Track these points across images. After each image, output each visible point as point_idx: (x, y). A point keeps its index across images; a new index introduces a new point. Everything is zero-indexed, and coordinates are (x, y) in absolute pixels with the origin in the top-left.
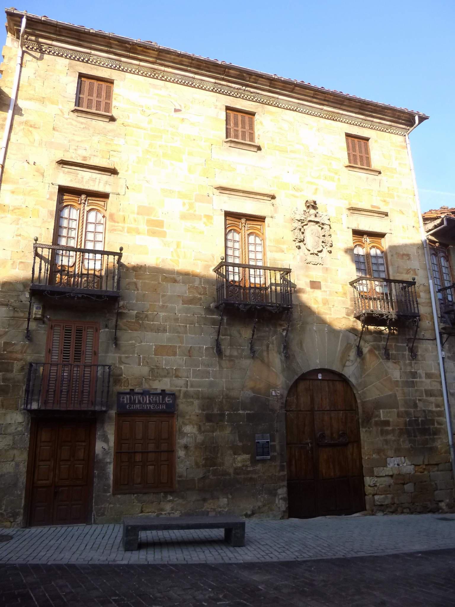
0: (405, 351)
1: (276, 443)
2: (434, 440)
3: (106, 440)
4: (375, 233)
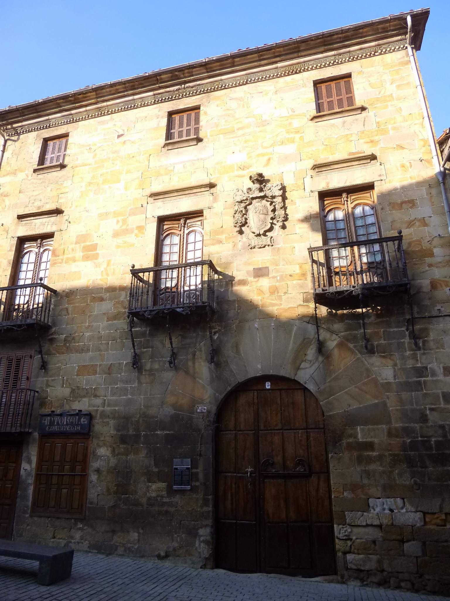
0: (404, 337)
1: (200, 470)
3: (29, 462)
4: (356, 187)
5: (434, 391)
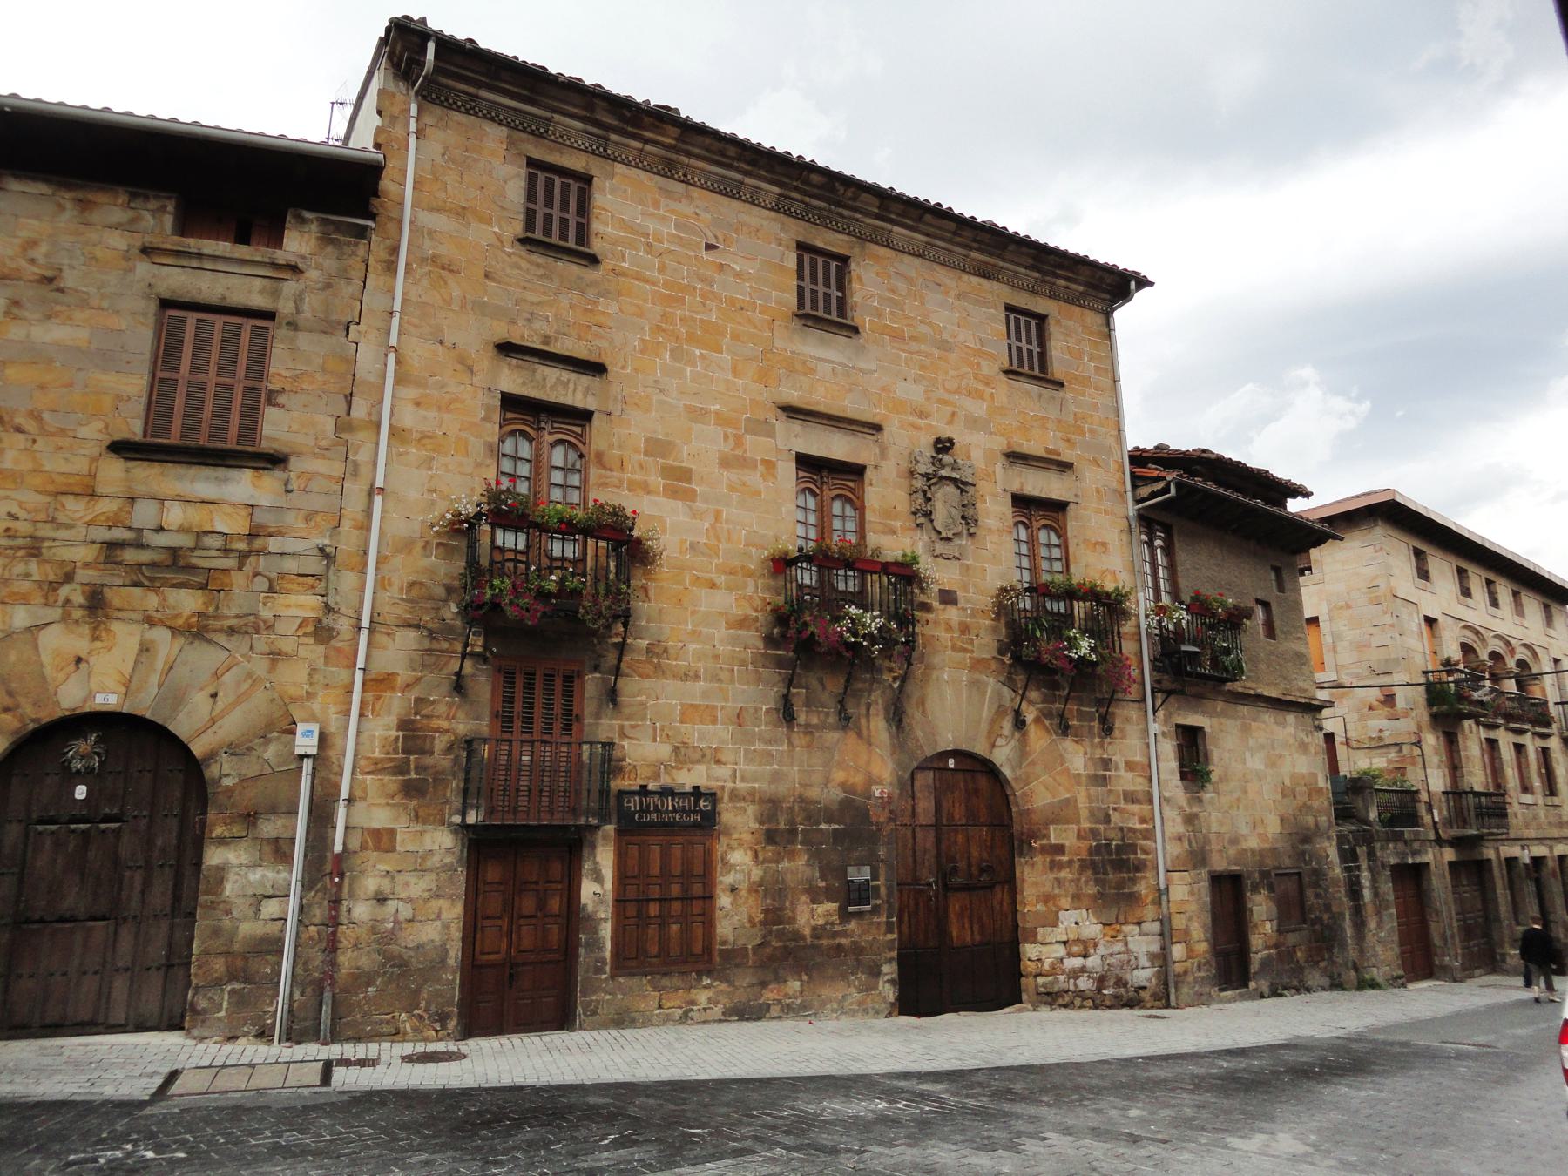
2: (1133, 881)
3: (598, 878)
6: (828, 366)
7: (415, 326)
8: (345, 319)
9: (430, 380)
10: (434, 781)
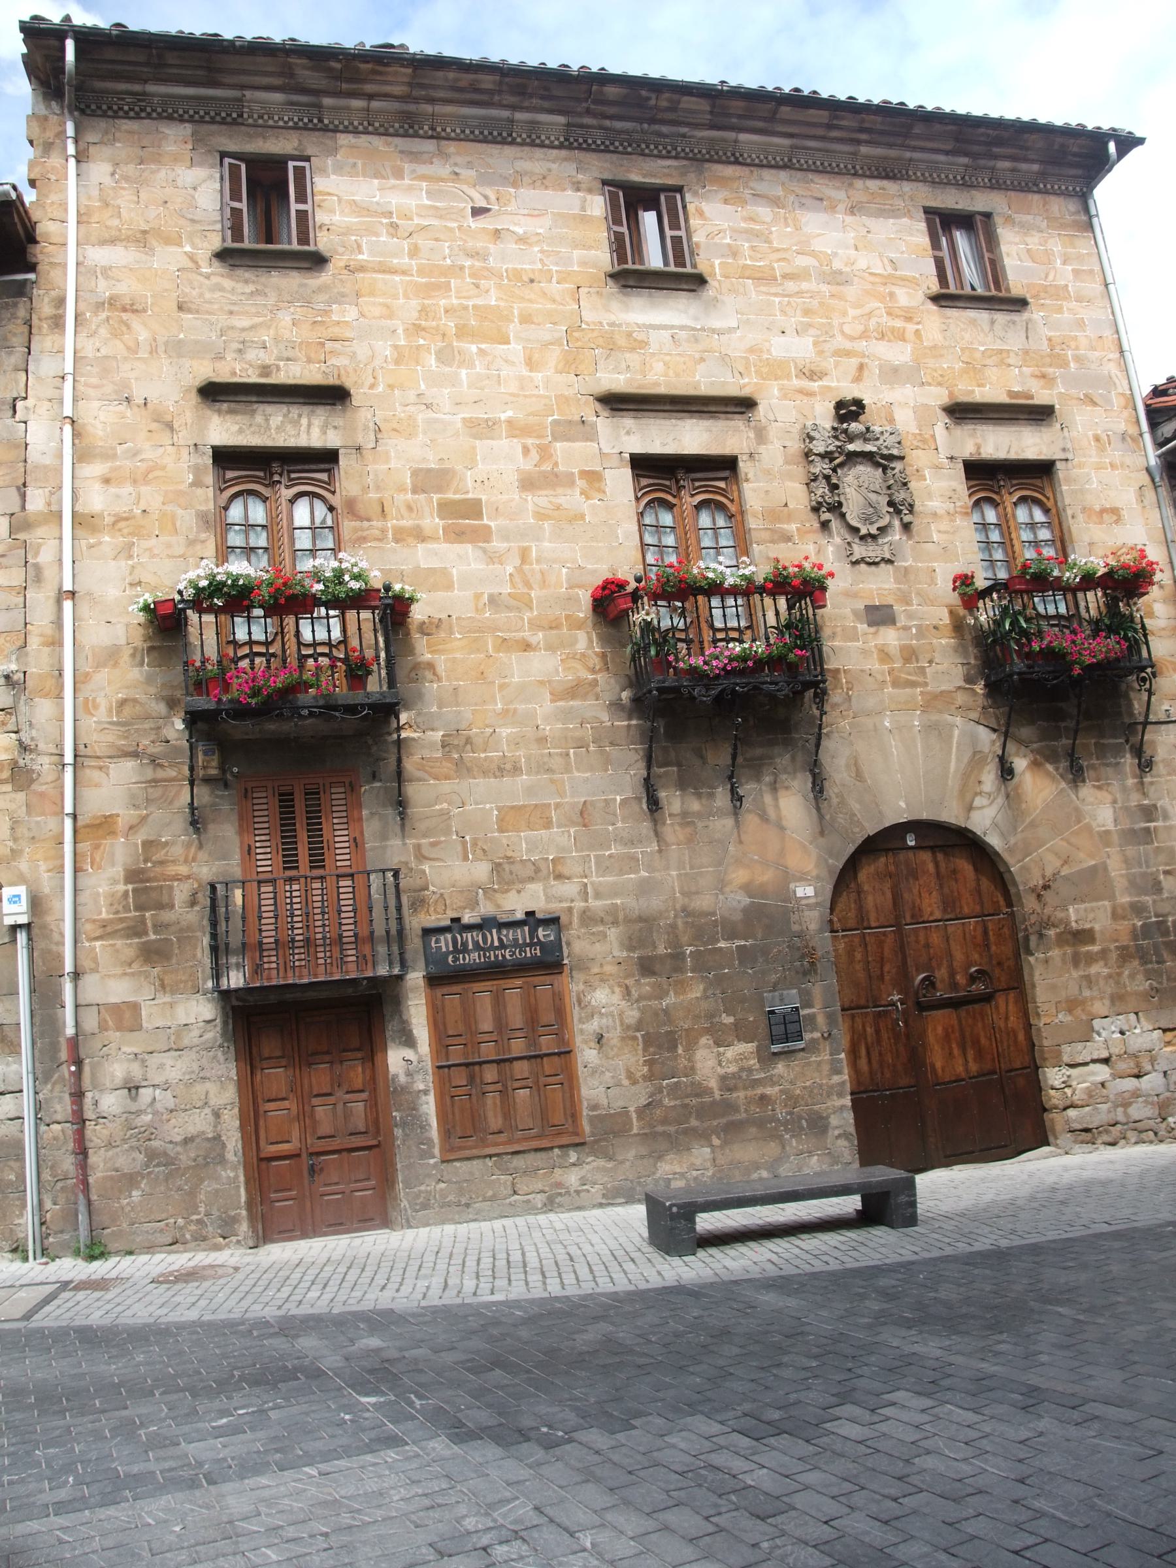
5: (1169, 844)
6: (666, 334)
7: (95, 387)
8: (9, 396)
9: (119, 449)
10: (178, 940)
